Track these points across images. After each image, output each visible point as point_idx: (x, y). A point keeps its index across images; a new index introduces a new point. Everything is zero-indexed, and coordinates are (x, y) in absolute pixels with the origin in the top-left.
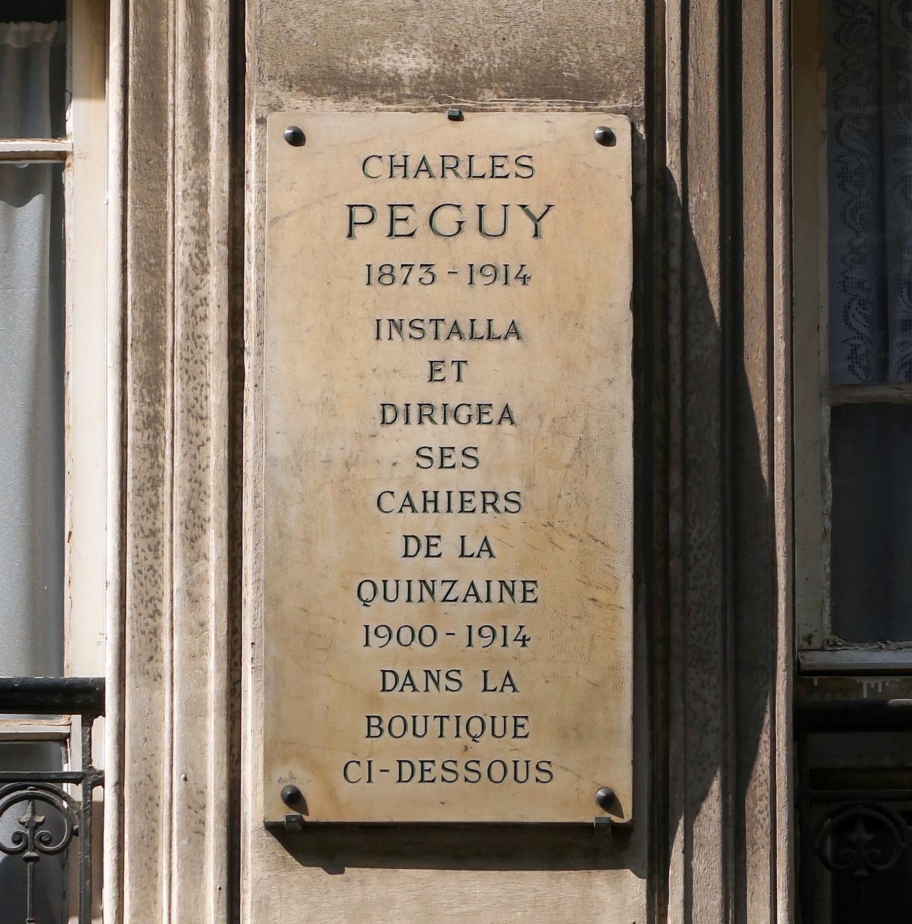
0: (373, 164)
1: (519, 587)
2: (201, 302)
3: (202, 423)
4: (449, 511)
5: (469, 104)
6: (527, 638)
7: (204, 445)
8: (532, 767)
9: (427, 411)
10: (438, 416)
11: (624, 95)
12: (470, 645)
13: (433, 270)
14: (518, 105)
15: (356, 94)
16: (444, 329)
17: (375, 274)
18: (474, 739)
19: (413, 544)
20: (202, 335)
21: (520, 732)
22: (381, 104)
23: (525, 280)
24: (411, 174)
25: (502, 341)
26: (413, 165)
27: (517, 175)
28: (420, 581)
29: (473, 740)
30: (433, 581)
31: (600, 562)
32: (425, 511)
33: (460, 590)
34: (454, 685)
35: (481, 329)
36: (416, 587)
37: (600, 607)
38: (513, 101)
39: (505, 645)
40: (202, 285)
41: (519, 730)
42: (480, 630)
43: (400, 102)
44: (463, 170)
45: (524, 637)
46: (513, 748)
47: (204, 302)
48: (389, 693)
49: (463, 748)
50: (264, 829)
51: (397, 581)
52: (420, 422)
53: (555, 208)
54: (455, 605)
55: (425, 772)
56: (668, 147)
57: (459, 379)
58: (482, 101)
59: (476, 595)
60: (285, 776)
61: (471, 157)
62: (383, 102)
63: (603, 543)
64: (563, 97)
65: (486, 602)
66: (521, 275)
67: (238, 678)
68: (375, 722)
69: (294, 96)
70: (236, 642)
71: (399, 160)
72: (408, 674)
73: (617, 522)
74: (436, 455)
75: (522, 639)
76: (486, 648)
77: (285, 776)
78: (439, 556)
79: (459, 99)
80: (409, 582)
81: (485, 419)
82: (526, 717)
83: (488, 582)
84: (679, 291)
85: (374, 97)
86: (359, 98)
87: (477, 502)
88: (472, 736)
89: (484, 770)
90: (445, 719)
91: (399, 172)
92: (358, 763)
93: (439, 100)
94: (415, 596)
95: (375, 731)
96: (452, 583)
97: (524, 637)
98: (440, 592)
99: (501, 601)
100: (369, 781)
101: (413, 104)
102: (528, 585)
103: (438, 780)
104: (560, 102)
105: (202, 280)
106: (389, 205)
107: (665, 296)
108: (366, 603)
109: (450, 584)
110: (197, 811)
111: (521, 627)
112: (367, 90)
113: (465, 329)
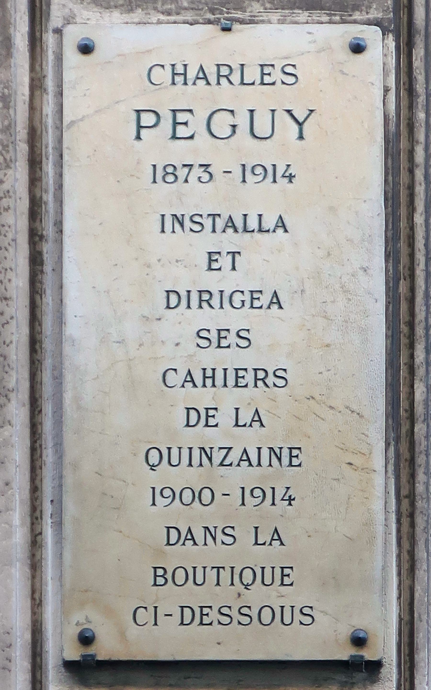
0: (157, 73)
1: (285, 453)
2: (4, 194)
3: (6, 303)
4: (225, 385)
5: (239, 15)
6: (292, 498)
7: (8, 323)
8: (297, 611)
9: (206, 297)
10: (215, 301)
11: (375, 7)
12: (243, 504)
13: (209, 170)
14: (282, 16)
15: (138, 6)
16: (220, 223)
17: (160, 173)
18: (246, 587)
19: (193, 415)
20: (5, 224)
21: (287, 581)
22: (162, 15)
23: (291, 178)
24: (190, 82)
25: (271, 234)
26: (192, 74)
27: (283, 83)
28: (200, 448)
29: (246, 588)
30: (211, 448)
31: (355, 430)
32: (204, 386)
33: (234, 456)
34: (230, 540)
35: (253, 224)
36: (196, 453)
37: (356, 470)
38: (278, 12)
39: (273, 504)
40: (5, 179)
41: (286, 578)
42: (252, 491)
43: (178, 14)
44: (236, 78)
45: (290, 497)
46: (279, 595)
47: (6, 194)
48: (172, 547)
49: (237, 596)
50: (62, 665)
51: (180, 448)
52: (200, 307)
53: (316, 113)
54: (230, 469)
55: (204, 617)
56: (414, 54)
57: (234, 268)
58: (250, 12)
59: (249, 460)
60: (82, 620)
61: (242, 65)
62: (163, 13)
63: (358, 414)
64: (322, 9)
65: (257, 466)
66: (287, 174)
67: (40, 530)
68: (160, 572)
69: (86, 9)
70: (36, 499)
71: (180, 69)
72: (190, 530)
73: (371, 395)
74: (214, 336)
75: (288, 498)
76: (257, 507)
77: (82, 620)
78: (216, 425)
79: (230, 11)
80: (190, 449)
81: (256, 304)
82: (292, 568)
83: (259, 449)
84: (423, 184)
85: (155, 9)
86: (142, 10)
87: (250, 378)
88: (150, 465)
89: (254, 613)
90: (221, 570)
91: (179, 79)
92: (146, 608)
93: (212, 11)
94: (196, 461)
95: (160, 581)
96: (226, 450)
97: (290, 497)
98: (217, 457)
99: (270, 465)
100: (156, 624)
101: (189, 16)
102: (293, 451)
103: (215, 623)
104: (319, 13)
105: (5, 175)
106: (171, 110)
107: (411, 188)
108: (153, 467)
109: (226, 450)
110: (4, 649)
111: (288, 488)
112: (150, 3)
113: (239, 224)
